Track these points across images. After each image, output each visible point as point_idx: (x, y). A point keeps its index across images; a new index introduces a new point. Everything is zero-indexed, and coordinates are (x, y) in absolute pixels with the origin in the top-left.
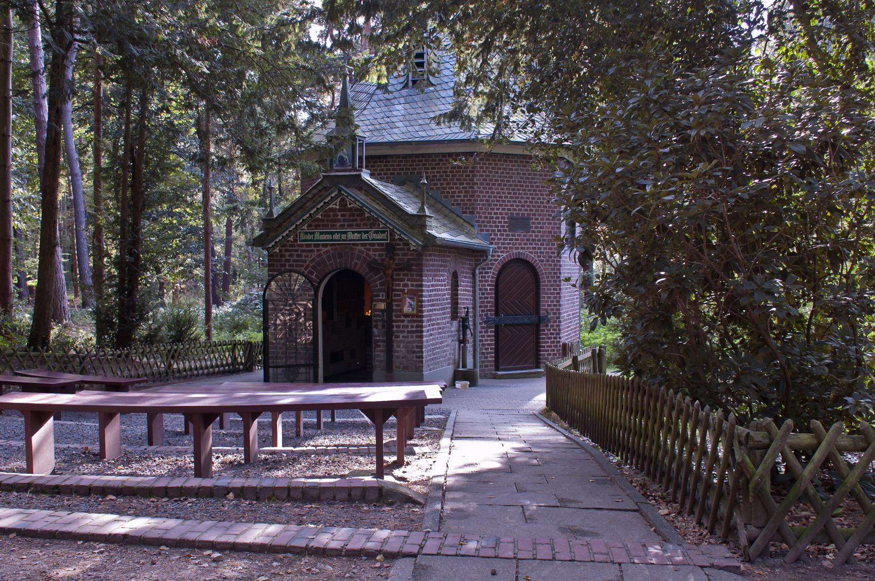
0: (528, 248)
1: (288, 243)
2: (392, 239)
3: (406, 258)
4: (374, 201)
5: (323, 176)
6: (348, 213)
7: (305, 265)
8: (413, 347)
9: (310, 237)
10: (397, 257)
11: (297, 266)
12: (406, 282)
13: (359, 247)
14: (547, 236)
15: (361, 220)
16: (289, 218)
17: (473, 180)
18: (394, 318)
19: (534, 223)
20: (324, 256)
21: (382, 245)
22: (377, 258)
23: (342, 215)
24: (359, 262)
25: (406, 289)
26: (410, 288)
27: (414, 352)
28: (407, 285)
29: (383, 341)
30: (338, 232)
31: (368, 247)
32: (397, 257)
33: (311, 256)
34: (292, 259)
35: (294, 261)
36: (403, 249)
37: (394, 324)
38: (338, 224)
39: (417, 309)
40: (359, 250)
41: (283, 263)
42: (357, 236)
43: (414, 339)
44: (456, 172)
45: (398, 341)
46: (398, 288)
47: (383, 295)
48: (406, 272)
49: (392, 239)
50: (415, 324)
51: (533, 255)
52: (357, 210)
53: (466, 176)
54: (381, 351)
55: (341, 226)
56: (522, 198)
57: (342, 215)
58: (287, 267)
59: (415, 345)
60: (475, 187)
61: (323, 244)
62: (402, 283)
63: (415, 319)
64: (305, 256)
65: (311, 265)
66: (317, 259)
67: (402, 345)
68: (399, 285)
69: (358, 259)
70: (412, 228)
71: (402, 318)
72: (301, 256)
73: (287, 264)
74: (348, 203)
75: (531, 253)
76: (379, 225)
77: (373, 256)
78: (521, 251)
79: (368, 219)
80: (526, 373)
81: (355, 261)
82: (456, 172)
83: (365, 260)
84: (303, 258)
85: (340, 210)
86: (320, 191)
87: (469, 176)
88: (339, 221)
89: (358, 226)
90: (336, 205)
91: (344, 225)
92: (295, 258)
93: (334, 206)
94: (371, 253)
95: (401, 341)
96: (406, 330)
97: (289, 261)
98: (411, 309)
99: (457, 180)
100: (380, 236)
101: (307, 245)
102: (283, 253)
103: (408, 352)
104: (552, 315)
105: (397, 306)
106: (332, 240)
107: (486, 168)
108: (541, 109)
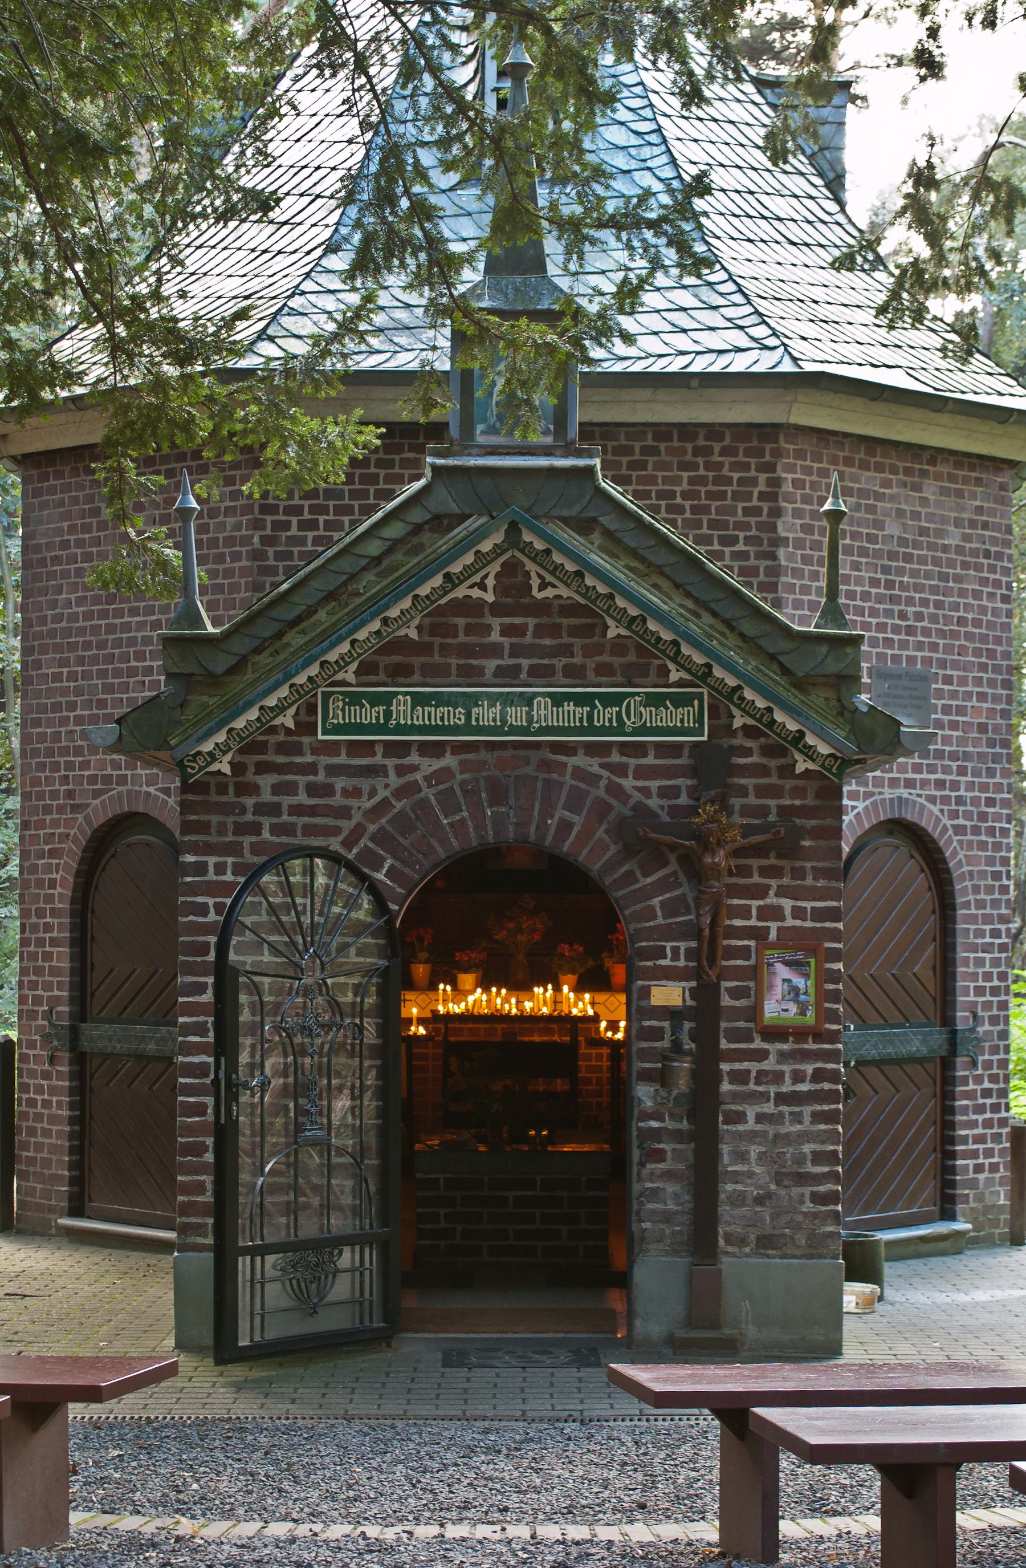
0: (924, 783)
1: (273, 739)
2: (722, 728)
3: (772, 803)
4: (643, 576)
5: (435, 468)
6: (531, 622)
7: (347, 826)
8: (800, 1160)
9: (371, 714)
10: (736, 802)
11: (309, 831)
12: (772, 900)
13: (580, 760)
14: (976, 742)
15: (589, 652)
16: (279, 635)
17: (773, 528)
18: (724, 1044)
19: (940, 694)
20: (429, 793)
21: (675, 750)
22: (653, 803)
23: (505, 631)
24: (578, 820)
25: (773, 926)
26: (790, 922)
27: (803, 1179)
28: (777, 914)
29: (677, 1136)
30: (493, 699)
31: (616, 758)
32: (736, 802)
33: (373, 793)
34: (287, 801)
35: (297, 810)
36: (763, 771)
37: (725, 1067)
38: (491, 665)
39: (818, 1006)
40: (576, 768)
41: (249, 817)
42: (573, 713)
43: (806, 1125)
44: (710, 496)
45: (740, 1135)
46: (738, 923)
47: (676, 951)
48: (772, 861)
49: (722, 728)
50: (809, 1068)
51: (935, 809)
52: (569, 609)
53: (746, 512)
54: (669, 1175)
55: (500, 671)
56: (910, 601)
57: (505, 631)
58: (266, 835)
59: (807, 1148)
60: (781, 553)
61: (658, 745)
62: (755, 903)
63: (811, 1046)
64: (345, 792)
65: (372, 828)
66: (399, 806)
67: (754, 1150)
68: (745, 913)
69: (575, 803)
70: (801, 685)
71: (758, 1044)
72: (328, 790)
73: (266, 822)
74: (535, 582)
75: (932, 799)
76: (665, 672)
77: (637, 796)
78: (904, 793)
79: (619, 646)
80: (922, 1239)
81: (561, 813)
82: (710, 496)
83: (602, 810)
84: (337, 800)
85: (496, 609)
86: (417, 529)
87: (756, 511)
88: (495, 651)
89: (575, 673)
90: (482, 586)
91: (518, 668)
92: (302, 798)
93: (476, 593)
94: (628, 783)
95: (753, 1136)
96: (773, 1090)
97: (274, 810)
98: (793, 1008)
99: (713, 525)
100: (669, 716)
101: (355, 748)
102: (250, 777)
103: (779, 1178)
104: (987, 1027)
105: (735, 993)
106: (468, 728)
107: (303, 526)
108: (922, 304)
